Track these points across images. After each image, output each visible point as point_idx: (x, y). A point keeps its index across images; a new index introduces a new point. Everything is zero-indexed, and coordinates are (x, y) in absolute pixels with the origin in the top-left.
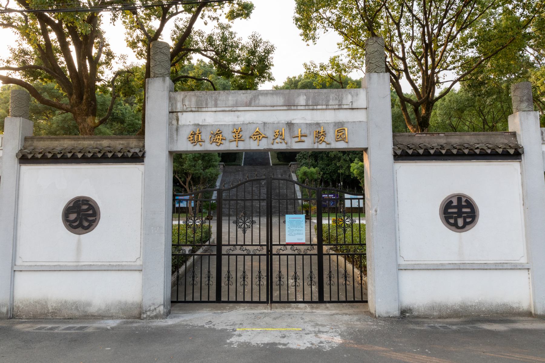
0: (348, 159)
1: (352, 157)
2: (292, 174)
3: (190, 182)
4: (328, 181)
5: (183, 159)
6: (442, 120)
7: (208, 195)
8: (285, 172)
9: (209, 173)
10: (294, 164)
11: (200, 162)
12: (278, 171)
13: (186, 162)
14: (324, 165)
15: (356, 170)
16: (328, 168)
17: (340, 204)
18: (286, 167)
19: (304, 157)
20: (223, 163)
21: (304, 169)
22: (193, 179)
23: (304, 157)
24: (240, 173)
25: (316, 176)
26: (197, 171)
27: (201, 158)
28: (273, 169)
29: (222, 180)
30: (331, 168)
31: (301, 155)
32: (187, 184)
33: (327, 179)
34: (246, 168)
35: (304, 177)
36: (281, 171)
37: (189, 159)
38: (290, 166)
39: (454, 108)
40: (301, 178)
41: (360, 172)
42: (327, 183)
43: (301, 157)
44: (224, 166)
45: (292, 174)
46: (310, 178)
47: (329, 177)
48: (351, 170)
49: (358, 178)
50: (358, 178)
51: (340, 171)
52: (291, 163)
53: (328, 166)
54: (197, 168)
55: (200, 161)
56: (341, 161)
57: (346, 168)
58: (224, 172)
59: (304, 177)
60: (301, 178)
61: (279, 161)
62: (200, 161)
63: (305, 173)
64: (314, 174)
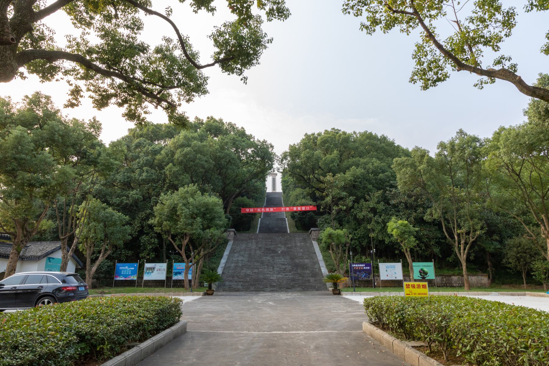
0: (380, 220)
1: (385, 219)
2: (313, 241)
3: (187, 245)
4: (357, 248)
5: (178, 216)
6: (510, 160)
7: (214, 265)
8: (304, 239)
9: (210, 234)
10: (315, 231)
11: (199, 219)
12: (296, 238)
13: (181, 220)
14: (351, 229)
15: (395, 230)
16: (356, 232)
17: (374, 276)
18: (305, 235)
19: (326, 222)
20: (234, 230)
21: (329, 230)
22: (191, 241)
23: (326, 222)
24: (254, 241)
25: (343, 240)
26: (194, 231)
27: (201, 215)
28: (290, 236)
29: (231, 249)
30: (360, 232)
31: (323, 220)
32: (183, 249)
33: (356, 246)
34: (261, 236)
35: (330, 241)
36: (300, 238)
37: (185, 216)
38: (310, 233)
39: (525, 143)
40: (325, 242)
41: (401, 232)
42: (355, 251)
43: (322, 221)
44: (235, 234)
45: (313, 241)
46: (336, 242)
47: (358, 243)
48: (389, 230)
49: (399, 241)
50: (399, 241)
51: (372, 235)
52: (312, 229)
53: (356, 230)
54: (195, 226)
55: (199, 218)
56: (372, 223)
57: (379, 232)
58: (235, 239)
59: (330, 241)
60: (325, 242)
61: (298, 229)
62: (199, 218)
63: (330, 236)
64: (341, 236)
